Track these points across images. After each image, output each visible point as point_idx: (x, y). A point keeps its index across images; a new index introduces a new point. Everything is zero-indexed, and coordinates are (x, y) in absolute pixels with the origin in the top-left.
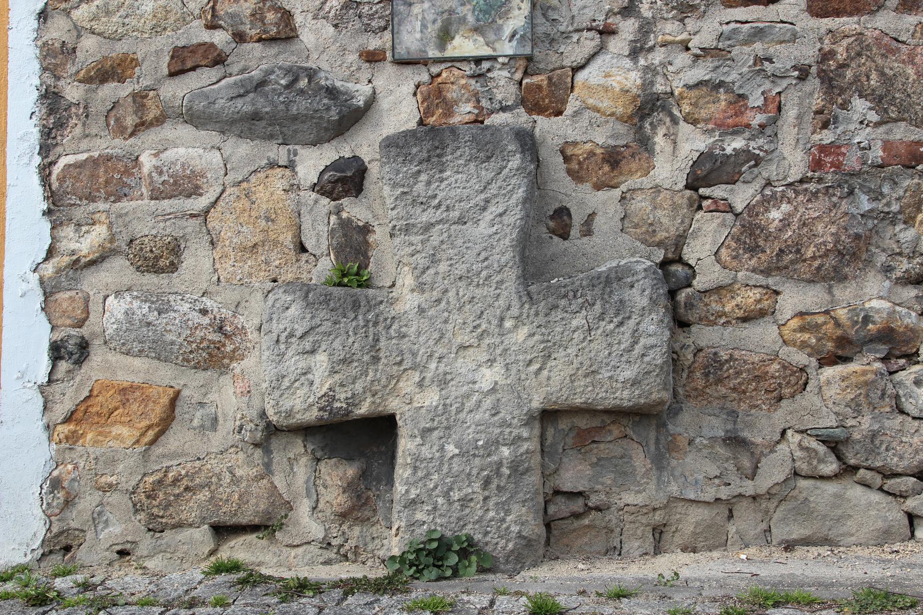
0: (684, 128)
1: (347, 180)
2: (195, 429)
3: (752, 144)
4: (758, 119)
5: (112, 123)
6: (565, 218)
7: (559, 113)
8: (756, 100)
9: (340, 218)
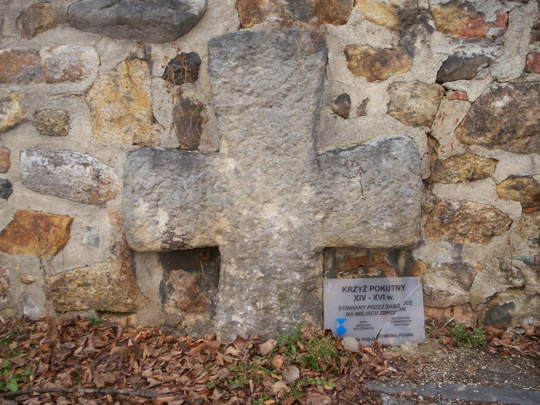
0: (437, 36)
1: (186, 70)
2: (84, 245)
3: (486, 50)
4: (492, 32)
5: (21, 27)
6: (346, 102)
7: (344, 22)
8: (491, 18)
9: (181, 99)
